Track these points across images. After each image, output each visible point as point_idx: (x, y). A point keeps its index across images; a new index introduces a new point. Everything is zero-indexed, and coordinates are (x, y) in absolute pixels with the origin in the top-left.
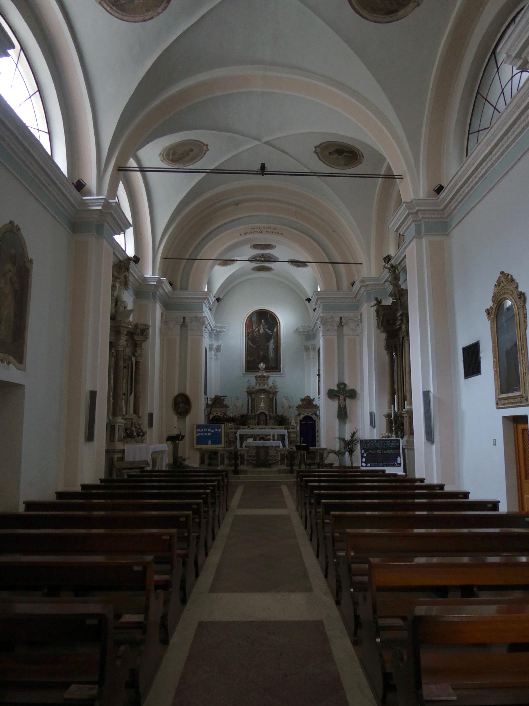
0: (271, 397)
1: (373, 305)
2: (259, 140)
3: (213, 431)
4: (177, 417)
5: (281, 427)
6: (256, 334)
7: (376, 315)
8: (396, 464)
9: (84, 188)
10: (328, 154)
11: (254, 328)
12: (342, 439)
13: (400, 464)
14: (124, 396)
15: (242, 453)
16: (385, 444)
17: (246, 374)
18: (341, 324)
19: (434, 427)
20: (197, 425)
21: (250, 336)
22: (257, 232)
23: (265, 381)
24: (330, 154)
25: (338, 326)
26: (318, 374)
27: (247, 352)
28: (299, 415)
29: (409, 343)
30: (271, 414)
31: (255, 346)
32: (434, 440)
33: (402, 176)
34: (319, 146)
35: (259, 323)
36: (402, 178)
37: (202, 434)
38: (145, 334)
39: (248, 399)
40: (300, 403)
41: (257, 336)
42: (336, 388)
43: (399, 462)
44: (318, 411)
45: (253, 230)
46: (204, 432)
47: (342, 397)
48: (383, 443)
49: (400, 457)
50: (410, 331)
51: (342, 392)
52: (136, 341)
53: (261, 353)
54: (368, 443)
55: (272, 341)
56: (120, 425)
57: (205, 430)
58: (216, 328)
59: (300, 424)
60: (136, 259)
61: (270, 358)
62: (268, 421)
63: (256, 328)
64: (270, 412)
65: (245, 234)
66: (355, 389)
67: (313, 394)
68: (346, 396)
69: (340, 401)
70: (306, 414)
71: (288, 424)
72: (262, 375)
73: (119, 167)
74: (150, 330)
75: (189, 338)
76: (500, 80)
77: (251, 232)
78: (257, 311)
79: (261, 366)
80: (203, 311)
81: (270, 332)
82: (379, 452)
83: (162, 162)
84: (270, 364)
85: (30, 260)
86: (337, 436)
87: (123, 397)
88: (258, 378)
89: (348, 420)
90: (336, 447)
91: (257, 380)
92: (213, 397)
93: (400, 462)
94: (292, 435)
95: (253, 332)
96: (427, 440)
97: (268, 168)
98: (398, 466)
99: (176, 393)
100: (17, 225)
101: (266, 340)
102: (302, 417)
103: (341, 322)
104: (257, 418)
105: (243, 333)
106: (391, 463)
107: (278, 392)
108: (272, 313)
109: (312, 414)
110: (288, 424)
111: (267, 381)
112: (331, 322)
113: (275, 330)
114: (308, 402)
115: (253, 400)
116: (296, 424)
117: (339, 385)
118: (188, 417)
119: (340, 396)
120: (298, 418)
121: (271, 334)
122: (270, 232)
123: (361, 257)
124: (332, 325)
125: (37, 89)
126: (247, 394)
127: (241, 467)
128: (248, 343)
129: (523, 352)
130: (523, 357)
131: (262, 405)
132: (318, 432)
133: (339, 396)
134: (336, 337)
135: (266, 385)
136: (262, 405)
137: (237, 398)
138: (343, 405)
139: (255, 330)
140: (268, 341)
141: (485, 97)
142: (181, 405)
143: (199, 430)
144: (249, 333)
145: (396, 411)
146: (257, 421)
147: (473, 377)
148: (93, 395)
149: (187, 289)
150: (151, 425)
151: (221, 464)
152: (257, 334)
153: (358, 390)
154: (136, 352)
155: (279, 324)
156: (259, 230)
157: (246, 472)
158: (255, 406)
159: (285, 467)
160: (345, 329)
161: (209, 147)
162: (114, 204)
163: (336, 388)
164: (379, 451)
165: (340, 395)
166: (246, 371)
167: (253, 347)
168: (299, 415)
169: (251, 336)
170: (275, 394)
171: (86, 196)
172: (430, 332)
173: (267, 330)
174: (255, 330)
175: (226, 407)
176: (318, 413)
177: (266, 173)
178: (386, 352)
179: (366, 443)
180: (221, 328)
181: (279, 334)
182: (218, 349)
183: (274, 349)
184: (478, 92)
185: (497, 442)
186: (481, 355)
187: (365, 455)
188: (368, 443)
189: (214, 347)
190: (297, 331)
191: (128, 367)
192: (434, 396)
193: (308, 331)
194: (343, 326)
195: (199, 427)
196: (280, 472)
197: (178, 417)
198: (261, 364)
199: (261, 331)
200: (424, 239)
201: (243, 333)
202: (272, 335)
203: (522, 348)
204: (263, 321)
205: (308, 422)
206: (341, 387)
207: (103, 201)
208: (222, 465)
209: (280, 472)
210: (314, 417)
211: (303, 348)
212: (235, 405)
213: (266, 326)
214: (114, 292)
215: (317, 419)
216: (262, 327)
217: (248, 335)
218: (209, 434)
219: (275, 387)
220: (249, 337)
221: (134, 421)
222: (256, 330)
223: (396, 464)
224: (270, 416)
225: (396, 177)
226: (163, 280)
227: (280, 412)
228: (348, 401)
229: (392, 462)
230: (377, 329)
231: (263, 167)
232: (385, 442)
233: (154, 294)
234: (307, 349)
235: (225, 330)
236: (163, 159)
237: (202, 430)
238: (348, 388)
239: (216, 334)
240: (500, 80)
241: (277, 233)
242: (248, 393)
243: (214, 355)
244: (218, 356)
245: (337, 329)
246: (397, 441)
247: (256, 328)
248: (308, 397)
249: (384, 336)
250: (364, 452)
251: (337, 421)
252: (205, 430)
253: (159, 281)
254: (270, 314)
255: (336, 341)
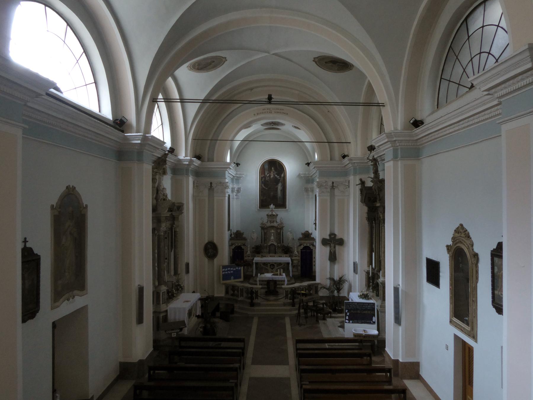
0: (279, 232)
1: (358, 184)
2: (268, 53)
3: (234, 269)
4: (207, 259)
5: (287, 255)
6: (268, 179)
7: (360, 193)
8: (372, 322)
9: (126, 124)
10: (325, 63)
11: (266, 174)
12: (332, 279)
13: (374, 323)
14: (166, 260)
15: (257, 290)
16: (363, 306)
17: (259, 210)
18: (333, 187)
19: (401, 314)
20: (222, 266)
21: (263, 180)
22: (267, 112)
23: (275, 219)
24: (326, 63)
25: (331, 189)
26: (314, 223)
27: (260, 193)
28: (300, 245)
29: (384, 228)
30: (279, 245)
31: (267, 189)
32: (401, 324)
33: (384, 104)
34: (317, 58)
35: (270, 170)
36: (384, 106)
37: (226, 273)
38: (180, 209)
39: (262, 232)
40: (301, 236)
41: (269, 181)
42: (328, 238)
43: (374, 320)
44: (315, 243)
45: (263, 111)
46: (228, 271)
47: (332, 245)
48: (362, 305)
49: (375, 317)
50: (386, 287)
51: (332, 241)
52: (174, 215)
53: (272, 193)
54: (351, 305)
55: (280, 184)
56: (163, 291)
57: (229, 269)
58: (236, 176)
59: (301, 252)
60: (172, 150)
61: (278, 198)
62: (277, 251)
63: (268, 174)
64: (278, 243)
65: (258, 114)
66: (343, 238)
67: (310, 228)
68: (337, 244)
69: (331, 247)
70: (305, 245)
71: (292, 252)
72: (272, 214)
73: (154, 99)
74: (185, 206)
75: (216, 199)
76: (470, 49)
77: (263, 113)
78: (269, 161)
79: (271, 206)
80: (226, 177)
81: (279, 177)
82: (359, 312)
83: (190, 71)
84: (278, 202)
85: (85, 206)
86: (328, 276)
87: (165, 251)
88: (269, 216)
89: (337, 262)
90: (328, 283)
91: (268, 218)
92: (235, 231)
93: (374, 321)
94: (295, 262)
95: (265, 177)
96: (395, 323)
97: (275, 98)
98: (373, 324)
99: (206, 241)
100: (73, 186)
101: (275, 183)
102: (302, 247)
103: (333, 186)
104: (268, 248)
105: (257, 178)
106: (367, 321)
107: (284, 227)
108: (280, 162)
109: (310, 245)
110: (292, 252)
111: (276, 218)
112: (325, 185)
113: (282, 175)
114: (307, 236)
115: (265, 234)
116: (298, 253)
117: (330, 235)
118: (215, 260)
119: (331, 244)
120: (299, 248)
121: (279, 178)
122: (278, 112)
123: (350, 139)
124: (326, 188)
125: (82, 51)
126: (261, 228)
127: (256, 301)
128: (261, 186)
129: (474, 299)
130: (473, 304)
131: (272, 238)
132: (314, 258)
133: (330, 244)
134: (328, 198)
135: (275, 222)
136: (272, 238)
137: (253, 232)
138: (333, 251)
139: (267, 175)
140: (277, 184)
141: (457, 55)
142: (210, 250)
143: (224, 270)
144: (262, 178)
145: (373, 267)
146: (268, 250)
147: (434, 285)
148: (141, 290)
149: (213, 161)
150: (187, 272)
151: (240, 297)
152: (269, 179)
153: (345, 239)
154: (174, 224)
155: (285, 171)
156: (269, 111)
157: (259, 305)
158: (267, 238)
159: (289, 301)
160: (336, 191)
161: (227, 59)
162: (150, 138)
163: (328, 238)
164: (359, 312)
165: (331, 243)
166: (260, 208)
167: (265, 189)
168: (300, 245)
169: (264, 180)
170: (282, 228)
171: (128, 133)
172: (401, 222)
173: (276, 176)
174: (267, 175)
175: (245, 239)
176: (315, 244)
177: (272, 103)
178: (367, 222)
179: (349, 305)
180: (240, 174)
181: (285, 178)
182: (239, 191)
183: (281, 191)
184: (450, 47)
185: (448, 348)
186: (441, 274)
187: (348, 314)
188: (351, 305)
189: (236, 189)
190: (299, 176)
191: (169, 238)
192: (402, 290)
193: (308, 177)
194: (334, 189)
195: (224, 267)
196: (285, 305)
197: (208, 259)
198: (271, 205)
199: (272, 177)
200: (399, 162)
201: (257, 178)
202: (280, 179)
203: (473, 296)
204: (273, 168)
205: (307, 251)
206: (332, 236)
207: (141, 137)
208: (242, 297)
209: (285, 305)
210: (311, 247)
211: (304, 189)
212: (252, 237)
213: (275, 173)
214: (155, 184)
215: (314, 248)
216: (273, 173)
217: (262, 179)
218: (232, 272)
219: (282, 223)
220: (262, 181)
221: (174, 283)
222: (268, 175)
223: (372, 322)
224: (278, 246)
225: (380, 105)
226: (194, 160)
227: (285, 244)
228: (337, 247)
229: (369, 321)
230: (361, 203)
231: (270, 98)
232: (364, 304)
233: (187, 170)
234: (307, 190)
235: (243, 176)
236: (190, 69)
237: (226, 270)
238: (337, 238)
239: (237, 179)
240: (470, 49)
241: (283, 113)
242: (261, 228)
243: (236, 195)
244: (238, 196)
245: (329, 191)
246: (373, 305)
247: (268, 174)
248: (307, 231)
249: (366, 209)
250: (348, 312)
251: (328, 262)
252: (229, 269)
253: (191, 161)
254: (278, 162)
255: (329, 200)
